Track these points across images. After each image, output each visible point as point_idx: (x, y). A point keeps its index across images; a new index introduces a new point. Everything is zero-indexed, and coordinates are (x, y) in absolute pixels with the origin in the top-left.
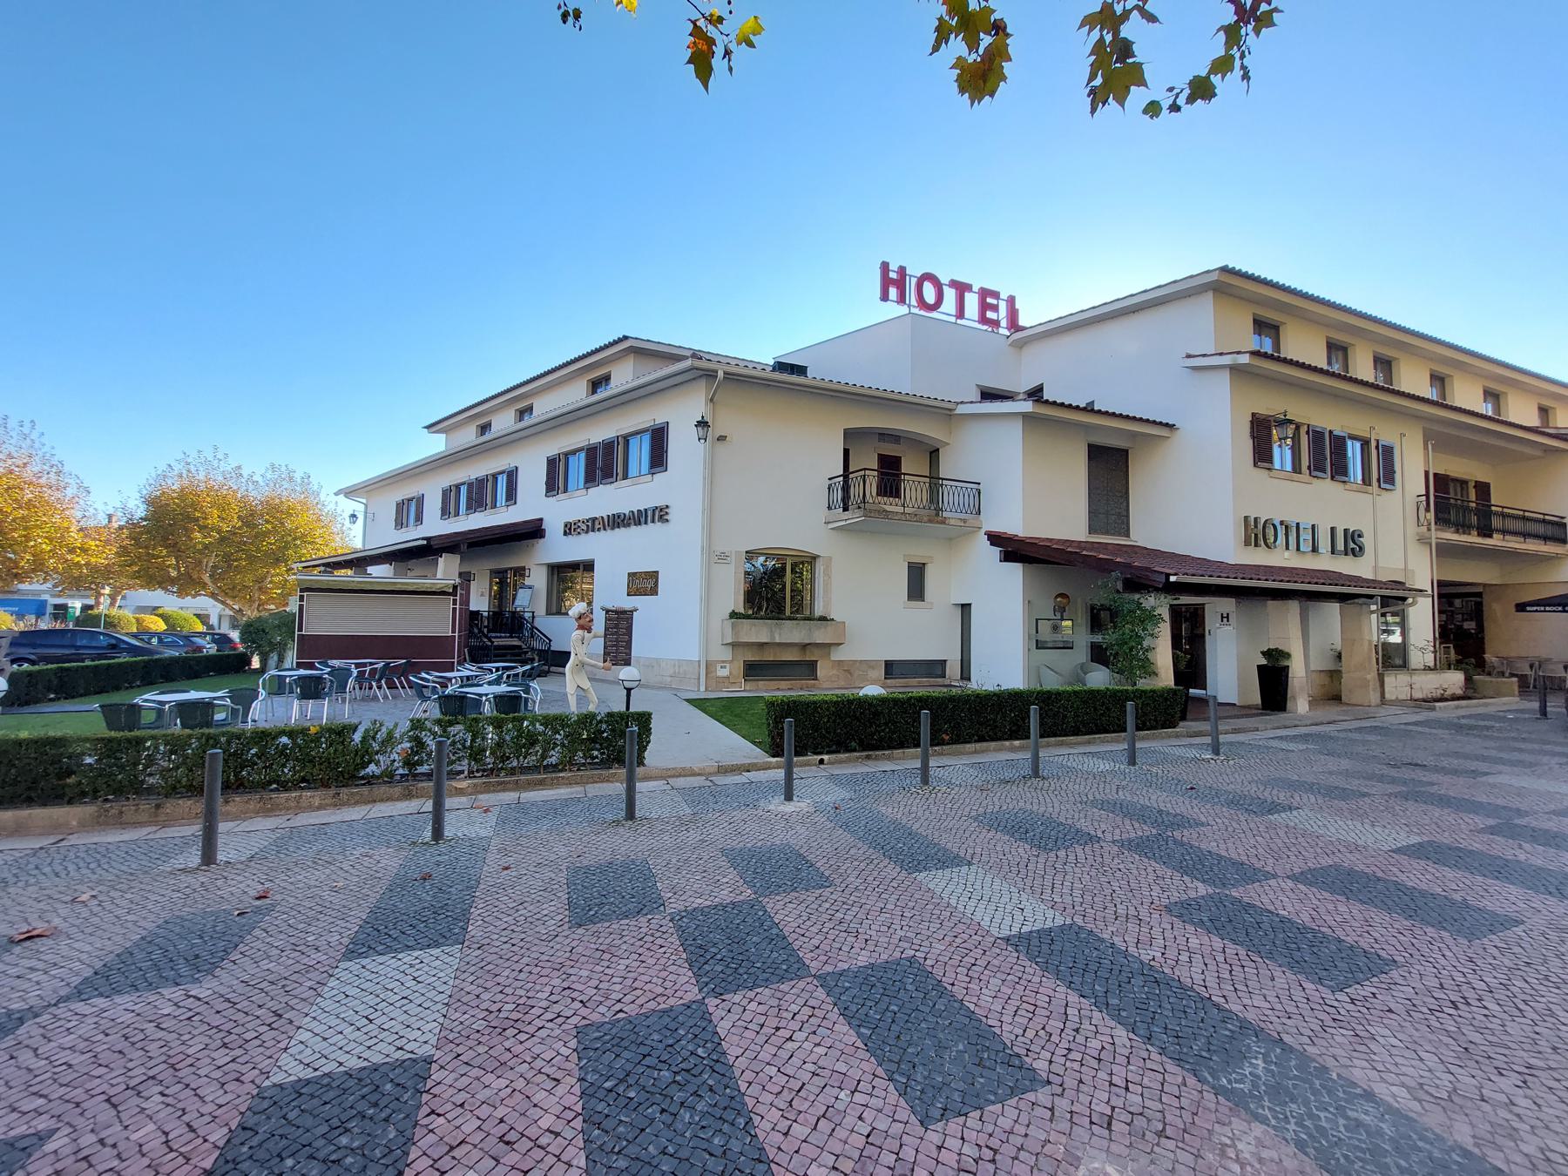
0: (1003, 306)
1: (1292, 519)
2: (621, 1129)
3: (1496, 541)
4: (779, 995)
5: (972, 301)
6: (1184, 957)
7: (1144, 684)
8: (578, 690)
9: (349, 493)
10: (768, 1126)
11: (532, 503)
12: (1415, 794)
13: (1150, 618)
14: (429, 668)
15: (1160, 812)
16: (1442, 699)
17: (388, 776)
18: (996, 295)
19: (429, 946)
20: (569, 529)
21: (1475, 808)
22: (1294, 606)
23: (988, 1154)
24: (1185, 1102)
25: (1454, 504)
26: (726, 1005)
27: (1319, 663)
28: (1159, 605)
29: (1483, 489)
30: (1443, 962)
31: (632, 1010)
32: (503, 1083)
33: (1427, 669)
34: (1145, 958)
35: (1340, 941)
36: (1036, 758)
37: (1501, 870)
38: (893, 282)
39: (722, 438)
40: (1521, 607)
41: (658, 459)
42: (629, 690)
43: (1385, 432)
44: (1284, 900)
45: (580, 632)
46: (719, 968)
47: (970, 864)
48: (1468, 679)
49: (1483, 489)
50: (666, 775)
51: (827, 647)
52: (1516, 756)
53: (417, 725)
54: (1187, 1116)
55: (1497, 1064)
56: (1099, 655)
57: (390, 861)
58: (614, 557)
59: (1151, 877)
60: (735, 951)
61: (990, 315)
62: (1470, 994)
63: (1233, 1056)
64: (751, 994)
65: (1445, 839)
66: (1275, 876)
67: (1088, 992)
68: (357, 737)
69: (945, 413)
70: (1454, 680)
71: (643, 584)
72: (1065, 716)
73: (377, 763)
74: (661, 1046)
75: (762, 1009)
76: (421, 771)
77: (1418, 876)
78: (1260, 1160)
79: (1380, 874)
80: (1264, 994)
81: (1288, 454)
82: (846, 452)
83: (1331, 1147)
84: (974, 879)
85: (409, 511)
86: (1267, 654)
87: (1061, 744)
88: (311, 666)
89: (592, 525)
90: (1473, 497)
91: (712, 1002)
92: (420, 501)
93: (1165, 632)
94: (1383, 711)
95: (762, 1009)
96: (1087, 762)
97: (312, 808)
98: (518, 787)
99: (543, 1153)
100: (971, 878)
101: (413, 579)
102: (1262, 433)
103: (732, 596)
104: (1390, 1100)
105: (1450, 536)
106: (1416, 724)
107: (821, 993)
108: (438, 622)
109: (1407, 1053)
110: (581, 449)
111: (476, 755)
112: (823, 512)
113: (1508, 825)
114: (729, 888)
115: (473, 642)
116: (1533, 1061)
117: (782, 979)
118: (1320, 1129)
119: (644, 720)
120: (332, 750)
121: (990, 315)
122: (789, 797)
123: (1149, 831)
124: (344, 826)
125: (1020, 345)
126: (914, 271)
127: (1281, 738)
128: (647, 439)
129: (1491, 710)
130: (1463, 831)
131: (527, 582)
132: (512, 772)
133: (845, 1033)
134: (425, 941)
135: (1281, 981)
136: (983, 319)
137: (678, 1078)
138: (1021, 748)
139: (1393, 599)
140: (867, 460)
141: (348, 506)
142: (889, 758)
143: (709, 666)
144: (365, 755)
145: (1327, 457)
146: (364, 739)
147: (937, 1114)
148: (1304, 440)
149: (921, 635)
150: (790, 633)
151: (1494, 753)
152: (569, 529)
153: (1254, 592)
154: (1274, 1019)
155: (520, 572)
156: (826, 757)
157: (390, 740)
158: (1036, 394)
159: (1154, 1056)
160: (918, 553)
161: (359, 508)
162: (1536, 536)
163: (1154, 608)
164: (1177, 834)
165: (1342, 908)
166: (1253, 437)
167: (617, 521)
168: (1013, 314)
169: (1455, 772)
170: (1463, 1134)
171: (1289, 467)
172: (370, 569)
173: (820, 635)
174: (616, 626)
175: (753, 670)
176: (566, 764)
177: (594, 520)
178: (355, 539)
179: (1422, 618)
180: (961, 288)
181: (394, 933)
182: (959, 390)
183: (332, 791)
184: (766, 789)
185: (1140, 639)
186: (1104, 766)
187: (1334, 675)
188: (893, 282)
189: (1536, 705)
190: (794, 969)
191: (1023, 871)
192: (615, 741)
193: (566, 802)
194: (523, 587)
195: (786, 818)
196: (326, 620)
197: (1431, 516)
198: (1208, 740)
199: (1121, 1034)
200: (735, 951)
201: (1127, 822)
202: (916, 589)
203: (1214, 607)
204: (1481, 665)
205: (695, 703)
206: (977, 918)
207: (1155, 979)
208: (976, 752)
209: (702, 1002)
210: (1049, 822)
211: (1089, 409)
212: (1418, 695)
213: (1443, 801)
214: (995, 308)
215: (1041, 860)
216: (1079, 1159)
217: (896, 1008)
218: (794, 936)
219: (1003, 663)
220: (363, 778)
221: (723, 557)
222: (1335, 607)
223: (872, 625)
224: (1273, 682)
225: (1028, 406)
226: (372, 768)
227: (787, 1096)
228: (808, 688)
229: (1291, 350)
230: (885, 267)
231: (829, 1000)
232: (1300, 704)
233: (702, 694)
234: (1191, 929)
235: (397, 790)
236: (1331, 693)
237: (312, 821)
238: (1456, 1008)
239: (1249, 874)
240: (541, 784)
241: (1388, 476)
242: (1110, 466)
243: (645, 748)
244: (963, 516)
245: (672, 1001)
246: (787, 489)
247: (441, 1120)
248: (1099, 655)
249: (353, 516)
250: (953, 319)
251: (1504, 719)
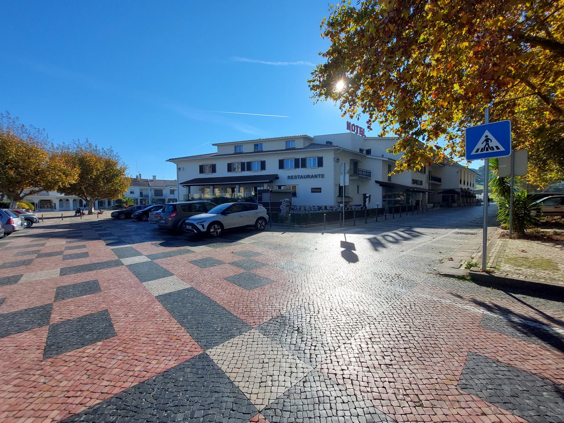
177: (299, 176)
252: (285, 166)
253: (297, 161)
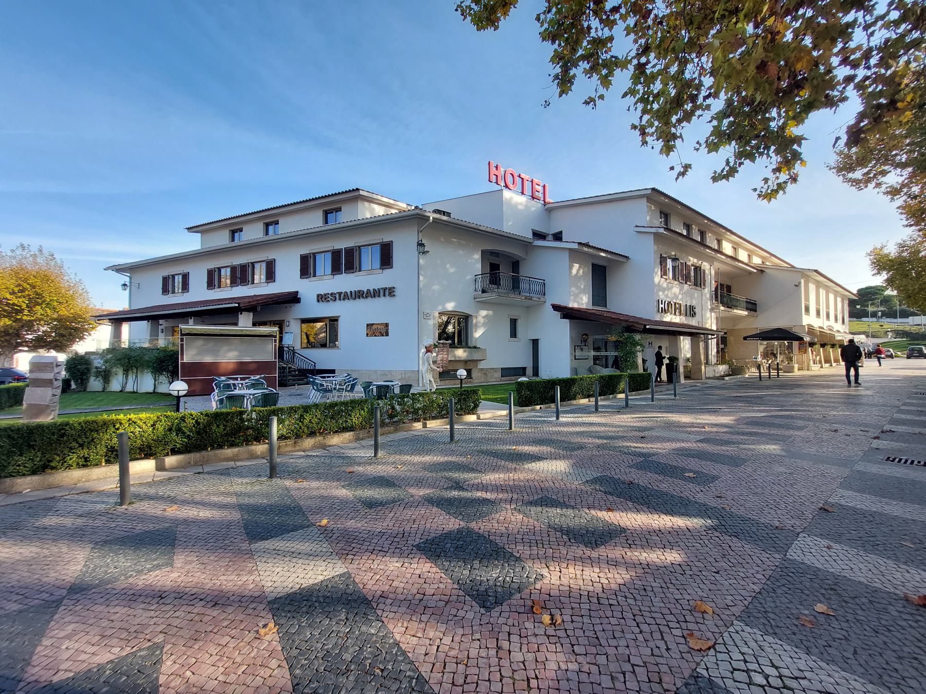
11: (288, 279)
20: (321, 298)
36: (124, 472)
40: (745, 338)
41: (386, 260)
167: (359, 295)
177: (340, 294)
202: (514, 334)
252: (356, 264)
253: (336, 254)
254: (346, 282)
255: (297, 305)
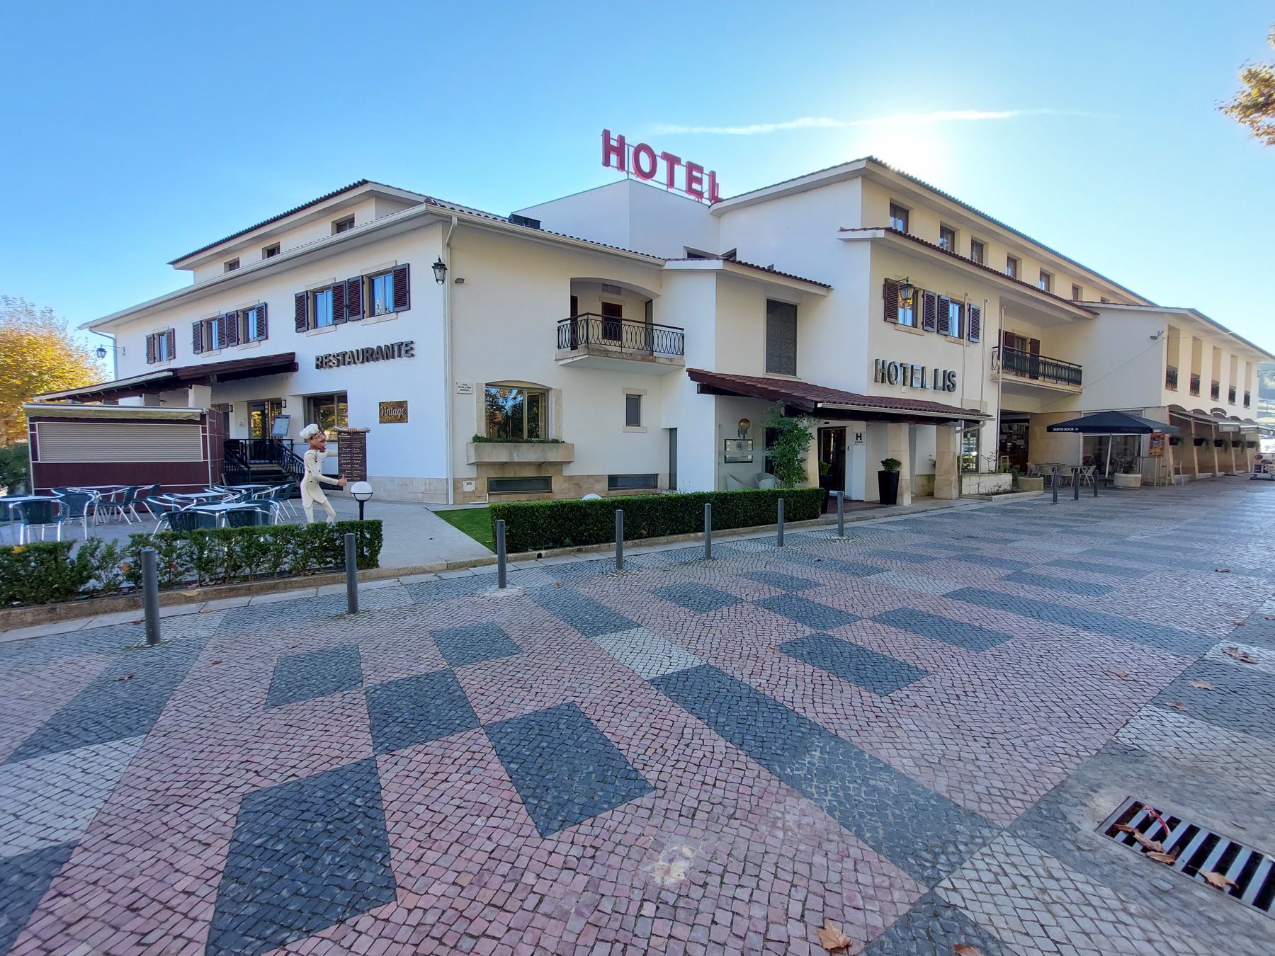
0: (706, 180)
1: (908, 362)
2: (260, 879)
3: (1040, 382)
4: (446, 745)
5: (680, 173)
6: (783, 682)
7: (798, 487)
8: (313, 505)
9: (95, 327)
10: (402, 856)
11: (281, 338)
12: (968, 557)
13: (804, 436)
14: (170, 491)
15: (792, 578)
16: (997, 493)
17: (112, 589)
18: (700, 169)
19: (110, 739)
20: (322, 363)
21: (1000, 563)
22: (905, 427)
23: (590, 852)
24: (755, 790)
25: (1018, 355)
26: (394, 760)
27: (922, 469)
28: (811, 426)
29: (1035, 344)
30: (958, 669)
31: (303, 774)
32: (149, 854)
33: (991, 472)
34: (753, 685)
35: (894, 660)
36: (708, 543)
37: (1006, 603)
38: (613, 149)
39: (460, 281)
40: (1050, 429)
41: (402, 299)
42: (362, 503)
43: (975, 300)
44: (864, 635)
45: (313, 451)
46: (397, 729)
47: (639, 626)
48: (1015, 480)
49: (1035, 344)
50: (397, 574)
51: (559, 465)
52: (1035, 528)
53: (139, 540)
54: (754, 801)
55: (975, 733)
56: (770, 467)
57: (96, 666)
58: (364, 390)
59: (774, 624)
60: (414, 714)
61: (695, 186)
62: (969, 689)
63: (798, 749)
64: (421, 747)
65: (978, 586)
66: (860, 619)
67: (704, 714)
68: (73, 554)
69: (655, 267)
70: (1006, 479)
71: (395, 412)
72: (737, 513)
73: (98, 578)
74: (322, 801)
75: (427, 758)
76: (144, 585)
77: (957, 612)
78: (799, 826)
79: (931, 612)
80: (832, 704)
81: (909, 313)
82: (574, 301)
83: (852, 807)
84: (636, 635)
85: (159, 344)
86: (885, 463)
87: (734, 534)
88: (48, 493)
89: (343, 359)
90: (1028, 350)
91: (382, 758)
92: (171, 335)
93: (813, 445)
94: (959, 503)
95: (427, 758)
96: (747, 548)
97: (24, 624)
98: (250, 592)
99: (171, 913)
100: (637, 637)
101: (168, 408)
102: (891, 293)
103: (474, 420)
104: (901, 769)
105: (1012, 377)
106: (979, 510)
107: (484, 740)
108: (190, 448)
109: (919, 734)
110: (327, 288)
111: (204, 565)
112: (554, 351)
113: (1019, 575)
114: (429, 661)
115: (231, 468)
116: (996, 729)
117: (452, 732)
118: (848, 797)
119: (376, 527)
120: (43, 569)
121: (695, 186)
122: (502, 585)
123: (779, 592)
124: (58, 638)
125: (719, 214)
126: (632, 141)
127: (889, 523)
128: (390, 279)
129: (1025, 500)
130: (988, 579)
131: (285, 412)
132: (246, 579)
133: (496, 769)
134: (109, 735)
135: (847, 694)
136: (690, 190)
137: (330, 827)
138: (697, 539)
139: (972, 423)
140: (592, 306)
141: (96, 340)
142: (597, 551)
143: (457, 483)
144: (83, 571)
145: (934, 315)
146: (80, 556)
147: (555, 825)
148: (920, 300)
149: (634, 455)
150: (527, 453)
151: (1020, 527)
152: (322, 363)
153: (880, 416)
154: (836, 721)
155: (277, 404)
156: (543, 552)
157: (110, 555)
158: (730, 257)
159: (742, 758)
160: (635, 387)
161: (108, 344)
162: (1063, 379)
163: (806, 429)
164: (800, 594)
165: (901, 637)
166: (885, 298)
167: (369, 355)
168: (714, 186)
169: (995, 541)
170: (941, 787)
171: (909, 322)
172: (123, 402)
173: (553, 455)
174: (350, 446)
175: (497, 486)
176: (300, 570)
177: (344, 355)
178: (106, 373)
179: (990, 434)
180: (672, 161)
181: (75, 731)
182: (668, 249)
183: (47, 607)
184: (481, 581)
185: (796, 452)
186: (761, 548)
187: (931, 478)
188: (613, 149)
189: (1051, 495)
190: (468, 720)
191: (679, 629)
192: (350, 548)
193: (295, 603)
194: (280, 416)
195: (496, 602)
196: (61, 448)
197: (1000, 363)
198: (836, 526)
199: (721, 743)
200: (414, 714)
201: (766, 586)
203: (854, 428)
204: (1024, 470)
205: (442, 514)
206: (632, 667)
207: (757, 699)
208: (668, 543)
209: (373, 759)
210: (709, 591)
211: (770, 271)
212: (983, 491)
213: (983, 560)
214: (699, 181)
215: (695, 619)
216: (663, 845)
217: (545, 744)
218: (475, 695)
219: (700, 474)
220: (83, 593)
221: (465, 388)
222: (933, 428)
223: (595, 444)
224: (888, 482)
225: (718, 265)
226: (92, 583)
227: (428, 829)
228: (548, 498)
229: (914, 231)
230: (606, 134)
231: (490, 744)
232: (906, 499)
233: (451, 505)
234: (792, 660)
235: (121, 602)
236: (928, 491)
237: (22, 637)
238: (959, 699)
239: (843, 618)
240: (274, 588)
241: (975, 333)
242: (783, 318)
243: (377, 552)
244: (670, 356)
245: (344, 762)
246: (521, 330)
247: (68, 900)
248: (770, 467)
249: (101, 350)
250: (665, 188)
251: (1031, 505)
254: (355, 335)
255: (295, 374)
